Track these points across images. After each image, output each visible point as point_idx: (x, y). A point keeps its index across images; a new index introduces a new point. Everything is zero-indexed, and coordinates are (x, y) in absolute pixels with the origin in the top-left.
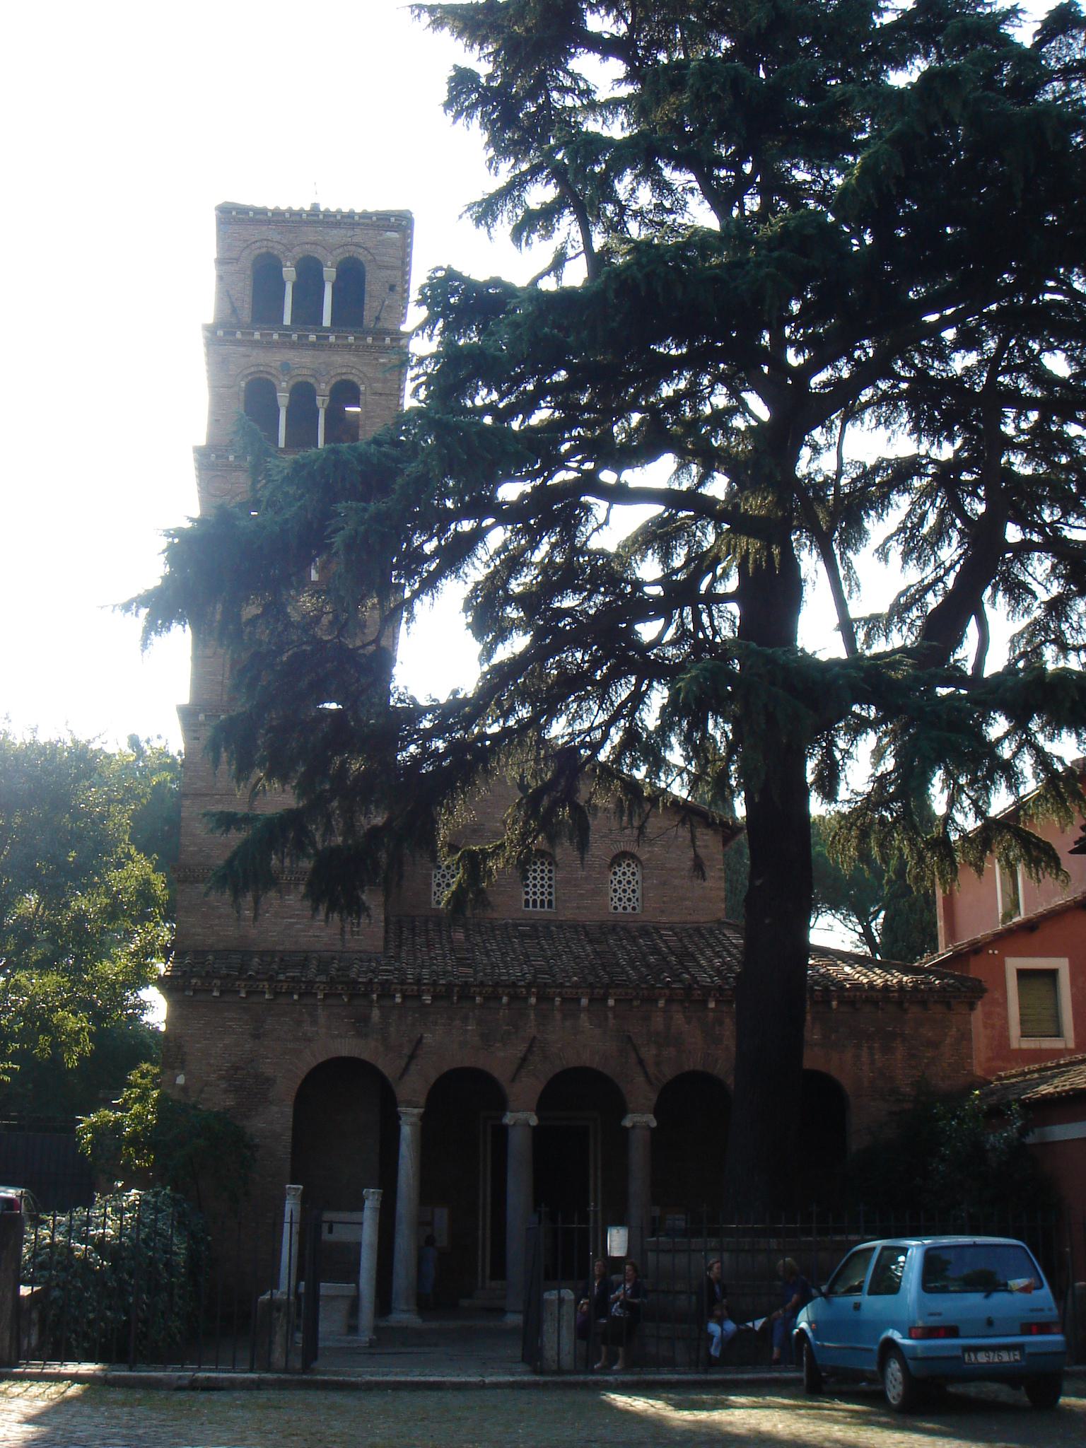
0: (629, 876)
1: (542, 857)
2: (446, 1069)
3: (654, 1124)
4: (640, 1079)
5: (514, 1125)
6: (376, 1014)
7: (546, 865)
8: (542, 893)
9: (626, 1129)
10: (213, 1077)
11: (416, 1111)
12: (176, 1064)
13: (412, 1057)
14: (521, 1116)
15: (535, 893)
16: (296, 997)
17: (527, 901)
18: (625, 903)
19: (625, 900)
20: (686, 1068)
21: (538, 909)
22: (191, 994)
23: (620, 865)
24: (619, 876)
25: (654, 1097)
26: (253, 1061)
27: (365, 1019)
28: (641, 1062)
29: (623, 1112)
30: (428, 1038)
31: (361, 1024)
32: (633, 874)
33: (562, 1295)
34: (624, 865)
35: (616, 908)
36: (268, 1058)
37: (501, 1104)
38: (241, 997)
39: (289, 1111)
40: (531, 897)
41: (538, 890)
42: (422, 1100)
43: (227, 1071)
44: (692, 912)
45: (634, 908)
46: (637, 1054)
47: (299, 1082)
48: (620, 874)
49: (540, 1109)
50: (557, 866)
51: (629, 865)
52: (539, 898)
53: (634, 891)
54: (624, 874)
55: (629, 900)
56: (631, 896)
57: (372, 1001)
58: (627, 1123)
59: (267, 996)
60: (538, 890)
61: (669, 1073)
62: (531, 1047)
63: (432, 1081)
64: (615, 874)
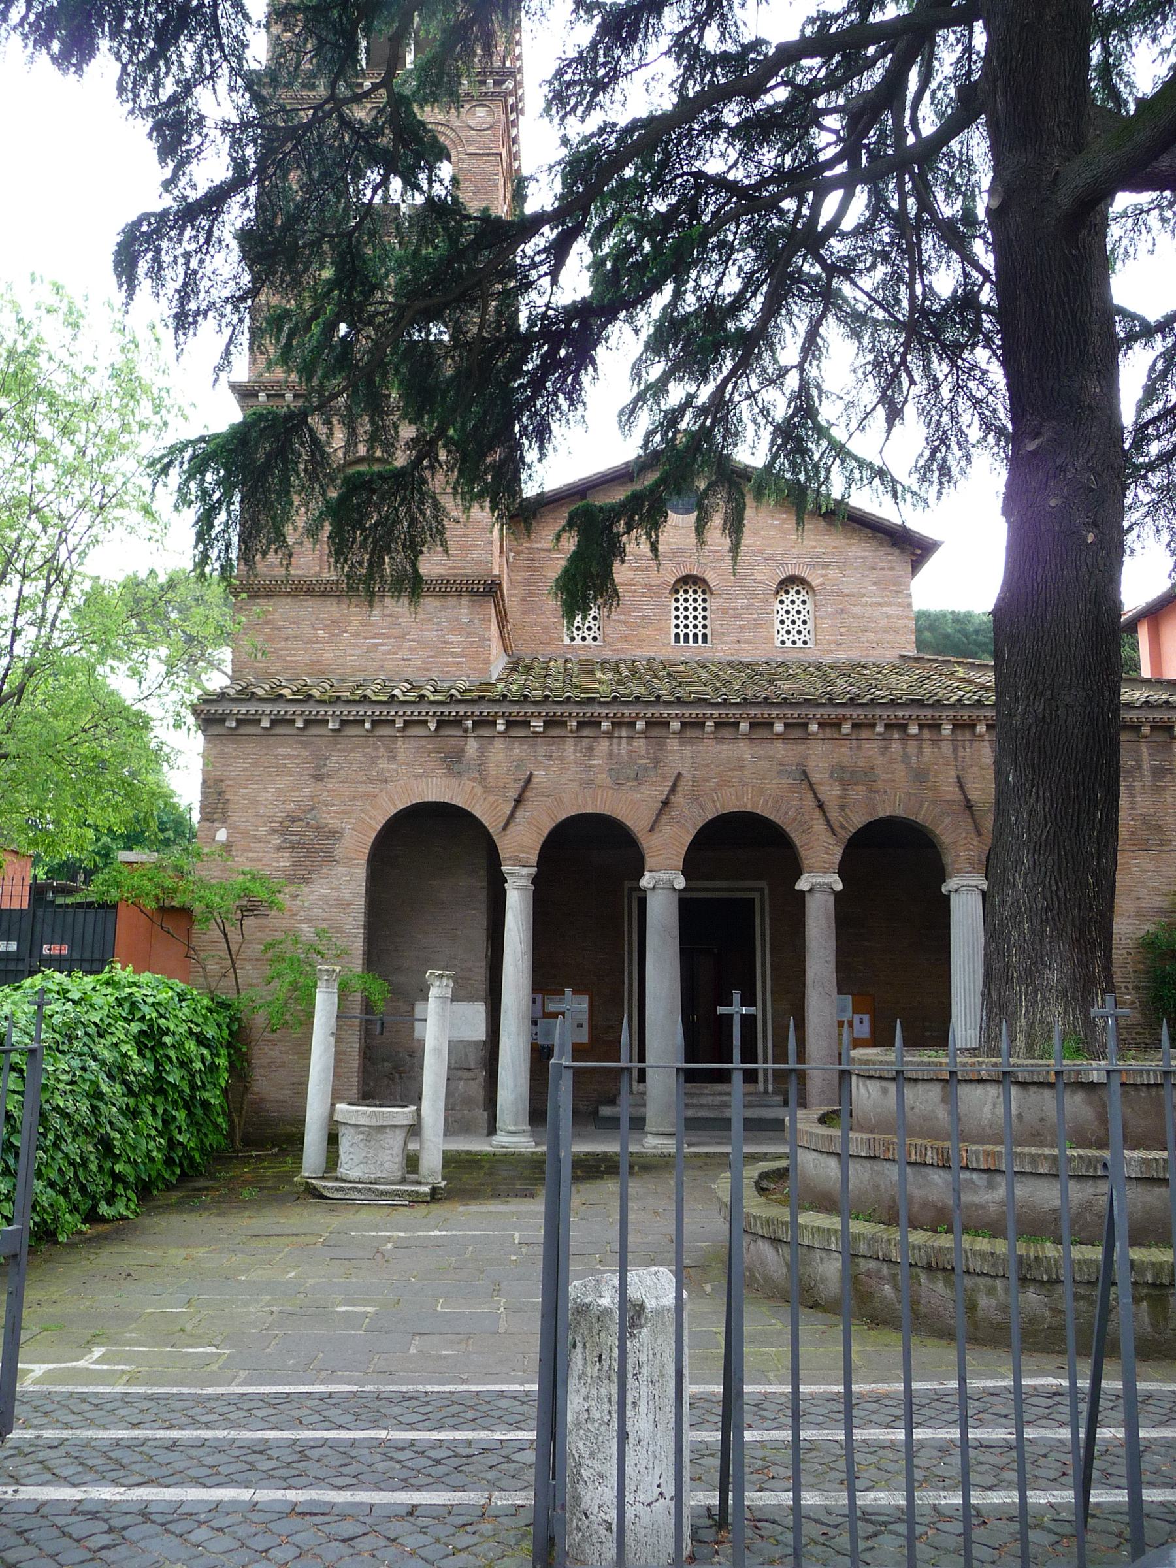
0: (798, 605)
1: (695, 584)
2: (563, 816)
3: (839, 886)
4: (819, 827)
5: (811, 890)
6: (472, 746)
7: (700, 593)
8: (695, 626)
9: (802, 892)
10: (263, 830)
11: (525, 871)
12: (216, 816)
13: (519, 801)
14: (662, 875)
15: (686, 626)
16: (368, 726)
17: (677, 635)
18: (794, 636)
19: (794, 632)
20: (881, 814)
21: (691, 644)
22: (234, 724)
23: (787, 592)
24: (787, 605)
25: (838, 853)
26: (313, 809)
27: (459, 753)
28: (821, 806)
29: (798, 874)
30: (540, 776)
31: (453, 762)
32: (804, 602)
33: (633, 1293)
34: (792, 592)
35: (783, 642)
36: (333, 805)
37: (638, 867)
38: (298, 728)
39: (361, 873)
40: (682, 631)
41: (691, 622)
42: (534, 858)
43: (281, 823)
44: (875, 645)
45: (805, 642)
46: (816, 797)
47: (374, 835)
48: (787, 602)
49: (688, 870)
50: (712, 593)
51: (798, 592)
52: (691, 632)
53: (804, 622)
54: (793, 602)
55: (799, 632)
56: (801, 628)
57: (466, 730)
58: (803, 885)
59: (330, 726)
60: (691, 622)
61: (858, 820)
62: (673, 790)
63: (546, 832)
64: (782, 602)
